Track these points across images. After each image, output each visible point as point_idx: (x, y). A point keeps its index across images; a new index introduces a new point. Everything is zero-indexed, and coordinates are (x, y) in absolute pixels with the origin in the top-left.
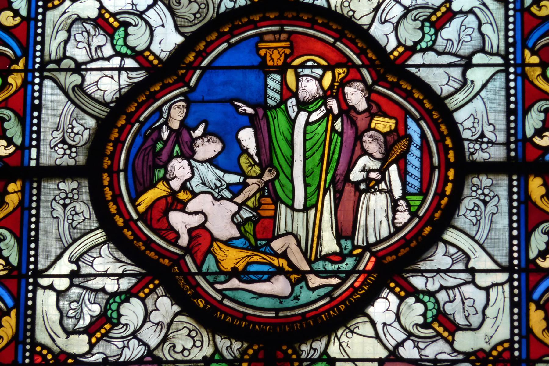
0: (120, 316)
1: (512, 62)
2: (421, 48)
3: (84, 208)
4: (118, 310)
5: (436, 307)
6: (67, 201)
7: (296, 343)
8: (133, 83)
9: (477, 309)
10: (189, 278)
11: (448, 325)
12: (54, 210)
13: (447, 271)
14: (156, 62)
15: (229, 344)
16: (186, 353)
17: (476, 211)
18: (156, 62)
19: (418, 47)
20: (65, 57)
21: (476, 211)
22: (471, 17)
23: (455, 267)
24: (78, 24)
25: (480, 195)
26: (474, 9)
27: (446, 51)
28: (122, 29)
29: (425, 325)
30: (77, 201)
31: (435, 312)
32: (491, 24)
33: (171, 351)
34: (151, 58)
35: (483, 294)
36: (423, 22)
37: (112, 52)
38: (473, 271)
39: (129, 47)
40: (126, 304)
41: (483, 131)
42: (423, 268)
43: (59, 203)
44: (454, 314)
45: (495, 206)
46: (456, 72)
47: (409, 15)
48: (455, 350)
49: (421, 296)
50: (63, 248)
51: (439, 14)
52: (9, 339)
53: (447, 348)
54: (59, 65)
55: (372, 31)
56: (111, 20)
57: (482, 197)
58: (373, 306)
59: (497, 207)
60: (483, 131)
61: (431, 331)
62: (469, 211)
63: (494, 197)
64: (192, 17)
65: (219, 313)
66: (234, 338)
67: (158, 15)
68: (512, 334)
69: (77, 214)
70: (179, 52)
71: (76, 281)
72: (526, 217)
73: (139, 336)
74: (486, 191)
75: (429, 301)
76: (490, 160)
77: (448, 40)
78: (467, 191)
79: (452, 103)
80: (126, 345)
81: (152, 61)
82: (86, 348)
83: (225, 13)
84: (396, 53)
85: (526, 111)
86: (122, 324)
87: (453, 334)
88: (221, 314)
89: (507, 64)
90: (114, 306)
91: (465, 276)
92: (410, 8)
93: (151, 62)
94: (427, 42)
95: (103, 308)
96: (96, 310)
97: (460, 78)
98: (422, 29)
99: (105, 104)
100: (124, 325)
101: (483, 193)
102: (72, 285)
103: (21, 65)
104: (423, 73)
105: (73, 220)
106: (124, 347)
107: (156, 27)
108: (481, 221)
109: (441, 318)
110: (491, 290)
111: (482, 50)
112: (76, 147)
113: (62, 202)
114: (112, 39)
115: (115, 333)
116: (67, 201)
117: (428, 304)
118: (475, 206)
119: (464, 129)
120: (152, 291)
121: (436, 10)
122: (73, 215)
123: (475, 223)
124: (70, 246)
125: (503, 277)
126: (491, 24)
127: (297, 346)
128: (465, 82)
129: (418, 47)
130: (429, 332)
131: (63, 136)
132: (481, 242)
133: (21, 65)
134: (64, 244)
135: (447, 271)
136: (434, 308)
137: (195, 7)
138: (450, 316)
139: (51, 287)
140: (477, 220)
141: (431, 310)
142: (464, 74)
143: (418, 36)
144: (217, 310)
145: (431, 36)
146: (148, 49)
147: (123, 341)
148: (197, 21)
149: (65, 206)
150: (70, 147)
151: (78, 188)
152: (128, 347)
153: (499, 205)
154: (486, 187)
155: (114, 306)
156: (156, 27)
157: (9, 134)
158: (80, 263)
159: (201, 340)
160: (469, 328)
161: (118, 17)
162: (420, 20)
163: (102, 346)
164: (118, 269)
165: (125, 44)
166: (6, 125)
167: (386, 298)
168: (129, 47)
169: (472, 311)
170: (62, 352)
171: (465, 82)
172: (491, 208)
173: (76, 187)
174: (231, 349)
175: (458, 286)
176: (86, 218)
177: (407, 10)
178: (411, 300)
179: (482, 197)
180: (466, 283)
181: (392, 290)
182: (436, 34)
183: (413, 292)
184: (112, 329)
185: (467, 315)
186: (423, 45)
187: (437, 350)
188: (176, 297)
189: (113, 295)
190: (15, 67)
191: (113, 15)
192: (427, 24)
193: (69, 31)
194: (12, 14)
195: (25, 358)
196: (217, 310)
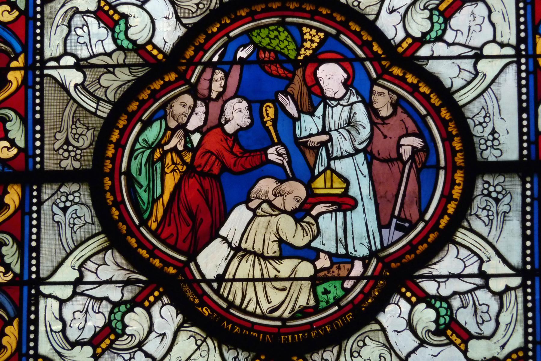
1: (524, 53)
3: (86, 213)
4: (122, 320)
5: (449, 314)
6: (68, 204)
8: (427, 267)
9: (491, 316)
10: (195, 285)
11: (104, 17)
12: (55, 214)
13: (460, 276)
17: (77, 133)
18: (160, 57)
21: (77, 133)
24: (487, 333)
25: (73, 151)
26: (70, 348)
29: (438, 332)
31: (117, 29)
34: (155, 52)
35: (69, 50)
36: (124, 333)
37: (113, 47)
40: (424, 31)
41: (65, 215)
42: (435, 273)
45: (58, 140)
46: (89, 277)
50: (492, 87)
51: (108, 341)
52: (13, 350)
54: (59, 63)
55: (379, 24)
56: (111, 12)
57: (71, 148)
58: (384, 312)
59: (55, 138)
60: (65, 215)
61: (443, 338)
62: (480, 210)
63: (507, 194)
64: (367, 340)
65: (226, 322)
66: (240, 348)
67: (405, 342)
68: (526, 341)
69: (480, 124)
70: (181, 44)
74: (66, 154)
75: (441, 307)
77: (99, 312)
78: (90, 152)
80: (132, 356)
81: (156, 56)
84: (405, 45)
86: (127, 335)
87: (466, 342)
88: (228, 325)
89: (518, 54)
91: (479, 281)
93: (155, 57)
94: (437, 31)
95: (107, 319)
97: (472, 70)
99: (456, 243)
100: (129, 335)
101: (69, 152)
102: (75, 294)
103: (20, 62)
104: (433, 67)
105: (74, 224)
107: (406, 329)
108: (71, 123)
109: (111, 24)
113: (62, 205)
114: (113, 32)
115: (119, 344)
118: (78, 139)
119: (475, 126)
120: (157, 299)
121: (110, 347)
122: (74, 219)
123: (78, 122)
124: (72, 251)
125: (516, 281)
126: (51, 330)
128: (477, 73)
130: (442, 339)
133: (20, 62)
134: (65, 250)
137: (365, 352)
138: (104, 26)
140: (75, 125)
141: (443, 316)
142: (82, 275)
143: (427, 26)
144: (223, 319)
145: (441, 24)
147: (130, 353)
148: (200, 11)
149: (65, 210)
150: (489, 195)
151: (79, 190)
153: (511, 204)
154: (67, 158)
155: (118, 316)
156: (406, 329)
157: (11, 136)
160: (480, 337)
161: (447, 341)
162: (127, 335)
164: (121, 276)
166: (8, 125)
167: (397, 304)
169: (486, 317)
173: (485, 152)
175: (470, 291)
178: (422, 306)
179: (71, 148)
180: (479, 287)
181: (403, 296)
182: (110, 321)
186: (123, 308)
188: (379, 36)
189: (115, 305)
190: (14, 64)
191: (451, 343)
192: (120, 332)
193: (69, 26)
194: (8, 8)
196: (223, 319)
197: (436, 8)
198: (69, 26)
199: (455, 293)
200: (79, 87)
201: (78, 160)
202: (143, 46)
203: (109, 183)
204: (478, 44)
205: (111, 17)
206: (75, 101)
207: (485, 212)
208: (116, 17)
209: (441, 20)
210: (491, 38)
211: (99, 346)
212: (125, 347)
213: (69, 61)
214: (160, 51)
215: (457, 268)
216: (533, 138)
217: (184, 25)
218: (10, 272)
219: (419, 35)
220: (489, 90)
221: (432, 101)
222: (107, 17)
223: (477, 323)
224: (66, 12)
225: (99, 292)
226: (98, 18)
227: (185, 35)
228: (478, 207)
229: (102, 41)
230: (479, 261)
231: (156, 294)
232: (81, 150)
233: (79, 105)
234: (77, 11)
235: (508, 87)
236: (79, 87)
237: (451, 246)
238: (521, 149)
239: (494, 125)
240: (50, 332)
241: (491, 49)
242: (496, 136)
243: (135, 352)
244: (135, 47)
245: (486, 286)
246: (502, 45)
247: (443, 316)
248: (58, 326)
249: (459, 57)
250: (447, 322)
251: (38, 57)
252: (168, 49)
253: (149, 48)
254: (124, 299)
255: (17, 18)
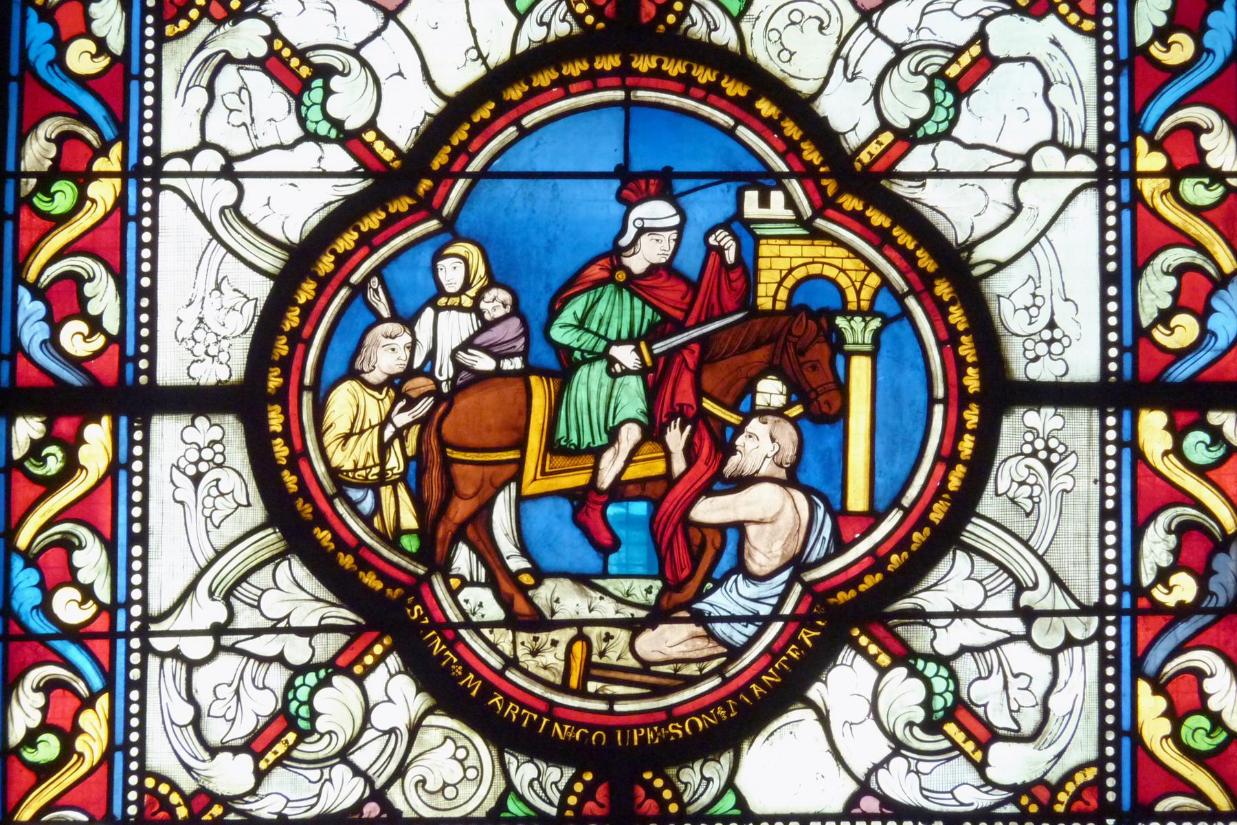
0: (929, 91)
2: (926, 134)
5: (952, 688)
7: (577, 36)
8: (911, 596)
13: (974, 614)
14: (864, 641)
15: (713, 34)
16: (450, 792)
17: (1031, 486)
18: (388, 155)
19: (920, 133)
20: (1053, 654)
21: (1031, 486)
22: (214, 738)
23: (990, 606)
27: (266, 666)
28: (318, 82)
29: (932, 726)
30: (220, 466)
31: (950, 698)
32: (173, 723)
33: (420, 789)
35: (210, 138)
36: (931, 78)
38: (1028, 615)
39: (919, 675)
43: (184, 473)
44: (985, 706)
46: (246, 618)
47: (904, 64)
48: (988, 782)
49: (920, 664)
53: (973, 777)
71: (227, 640)
72: (1138, 497)
73: (352, 757)
75: (936, 675)
76: (1066, 379)
77: (265, 687)
79: (271, 540)
82: (250, 782)
83: (528, 52)
85: (1137, 273)
86: (925, 75)
87: (983, 747)
89: (144, 633)
90: (303, 694)
91: (239, 167)
92: (904, 48)
93: (874, 640)
96: (266, 704)
98: (314, 715)
99: (969, 549)
100: (922, 73)
102: (218, 649)
103: (111, 162)
105: (1034, 296)
106: (918, 29)
109: (962, 715)
110: (1060, 656)
111: (191, 665)
112: (1022, 454)
113: (191, 470)
115: (307, 750)
116: (1047, 335)
117: (934, 680)
121: (959, 51)
124: (211, 563)
125: (1081, 628)
126: (173, 723)
127: (576, 30)
129: (920, 133)
130: (318, 58)
131: (1050, 478)
132: (1040, 552)
135: (974, 614)
136: (947, 690)
139: (1069, 152)
141: (941, 694)
145: (947, 109)
146: (883, 671)
147: (321, 769)
149: (197, 479)
150: (1034, 454)
152: (330, 780)
158: (233, 600)
159: (478, 765)
160: (1017, 737)
163: (280, 779)
164: (308, 615)
165: (927, 682)
168: (919, 675)
169: (233, 101)
170: (202, 791)
171: (1017, 208)
172: (1062, 481)
174: (709, 26)
175: (995, 645)
176: (239, 505)
177: (900, 53)
180: (1013, 638)
183: (349, 139)
184: (297, 742)
185: (1014, 707)
186: (311, 679)
187: (953, 784)
188: (822, 132)
190: (100, 165)
193: (210, 88)
195: (126, 803)
197: (941, 74)
198: (210, 88)
199: (964, 649)
200: (1031, 585)
201: (1031, 429)
202: (357, 134)
203: (967, 381)
204: (223, 658)
205: (294, 73)
206: (1033, 552)
207: (1026, 490)
208: (305, 72)
209: (950, 99)
210: (1047, 136)
211: (975, 60)
212: (321, 755)
213: (209, 161)
214: (863, 651)
215: (970, 597)
216: (1128, 341)
217: (810, 704)
218: (91, 602)
219: (904, 124)
220: (1043, 240)
221: (921, 264)
222: (278, 63)
223: (1011, 711)
224: (206, 60)
225: (266, 645)
226: (988, 725)
227: (808, 685)
228: (1013, 481)
229: (980, 678)
230: (1013, 587)
231: (378, 649)
232: (1022, 454)
233: (1025, 543)
234: (228, 59)
235: (1079, 238)
236: (227, 211)
237: (960, 554)
238: (1105, 359)
239: (1053, 314)
240: (169, 723)
241: (198, 648)
242: (1057, 334)
243: (332, 766)
244: (912, 662)
245: (230, 159)
246: (176, 654)
247: (941, 694)
248: (187, 713)
249: (256, 632)
250: (949, 704)
251: (1110, 646)
252: (846, 654)
253: (884, 660)
254: (314, 661)
255: (106, 69)
